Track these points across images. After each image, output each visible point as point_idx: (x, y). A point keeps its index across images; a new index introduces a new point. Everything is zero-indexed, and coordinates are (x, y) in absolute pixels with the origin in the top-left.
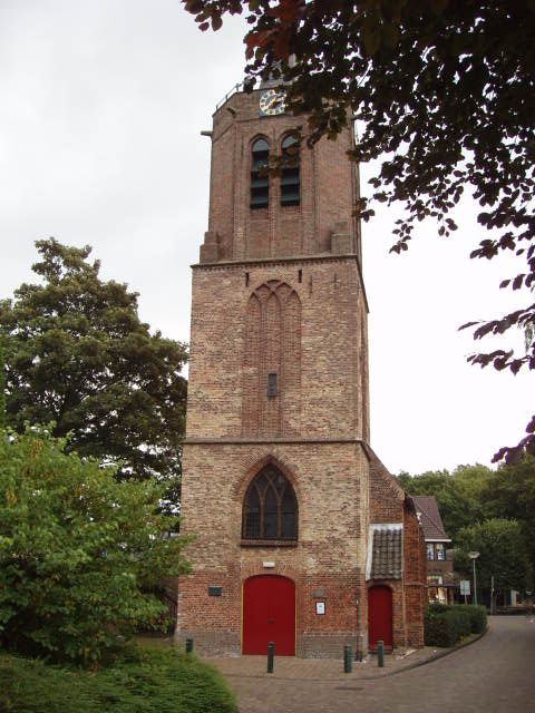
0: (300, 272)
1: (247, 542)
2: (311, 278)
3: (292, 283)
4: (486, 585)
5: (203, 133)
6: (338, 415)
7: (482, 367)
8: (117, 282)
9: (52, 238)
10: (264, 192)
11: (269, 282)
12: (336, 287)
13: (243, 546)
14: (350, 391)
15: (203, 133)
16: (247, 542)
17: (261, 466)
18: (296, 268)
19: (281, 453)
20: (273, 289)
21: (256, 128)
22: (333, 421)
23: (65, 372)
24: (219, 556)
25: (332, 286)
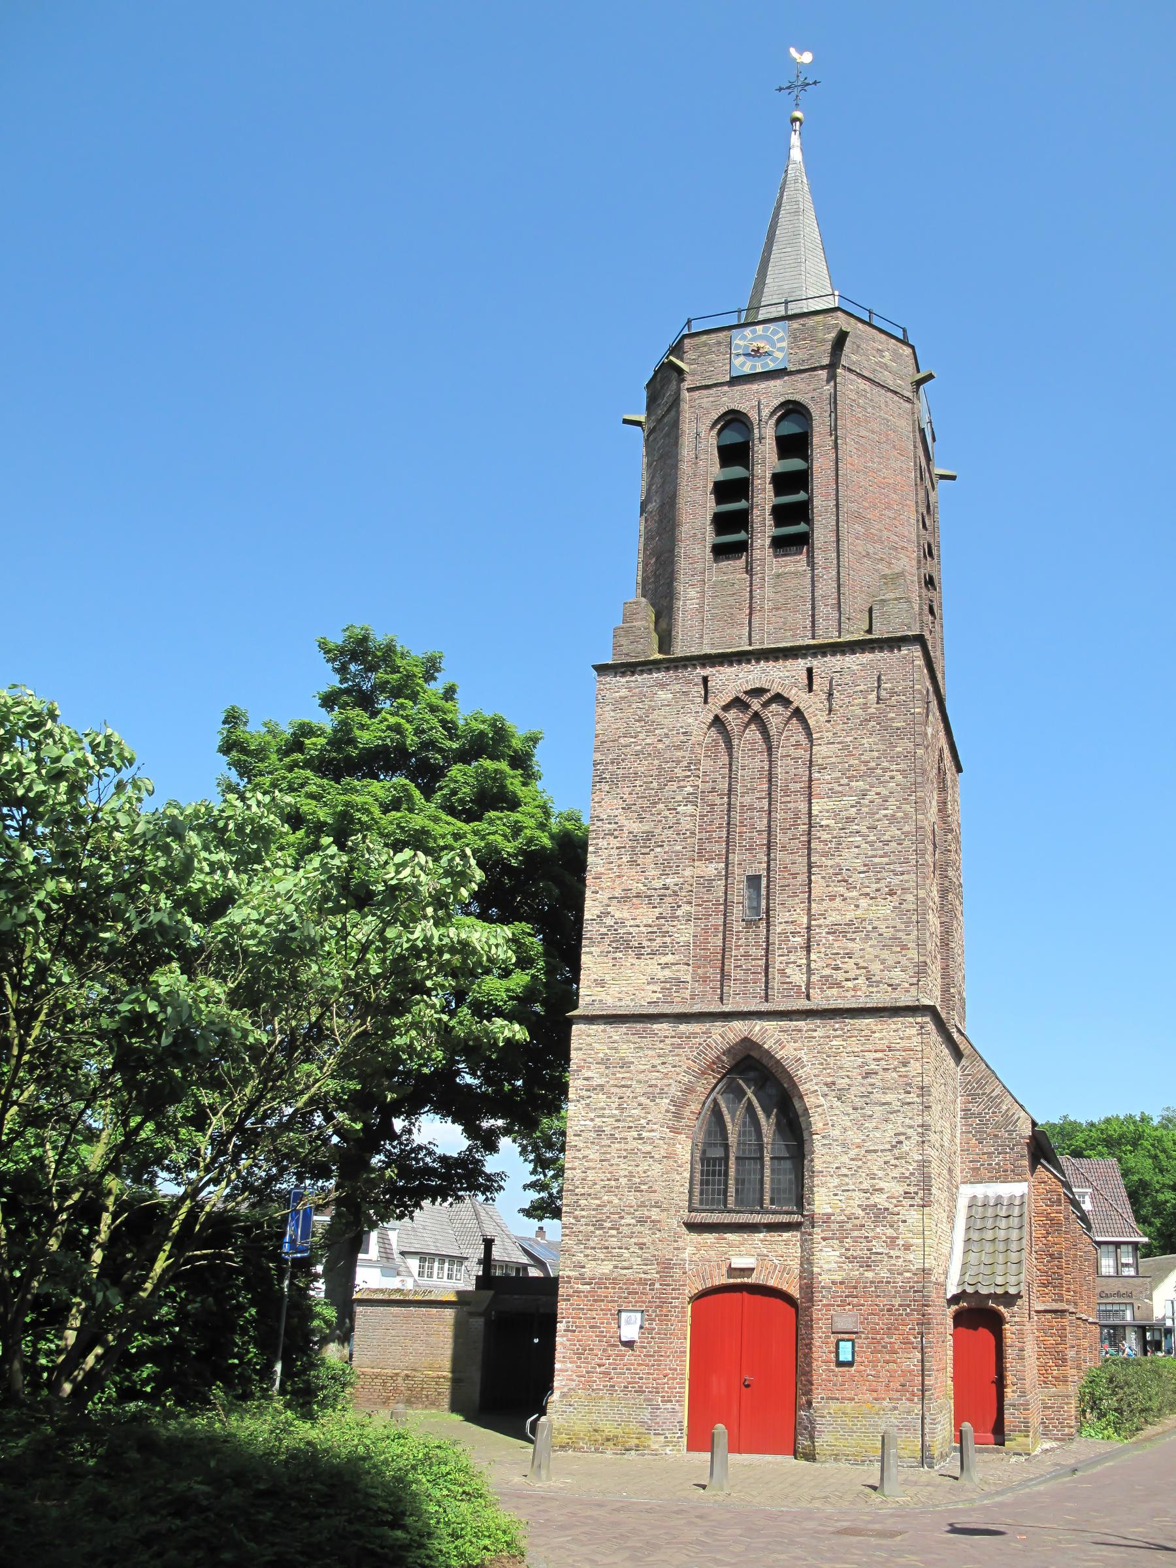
0: (810, 671)
1: (700, 1217)
6: (885, 954)
13: (692, 1227)
18: (801, 664)
22: (876, 967)
24: (641, 1246)
25: (873, 697)
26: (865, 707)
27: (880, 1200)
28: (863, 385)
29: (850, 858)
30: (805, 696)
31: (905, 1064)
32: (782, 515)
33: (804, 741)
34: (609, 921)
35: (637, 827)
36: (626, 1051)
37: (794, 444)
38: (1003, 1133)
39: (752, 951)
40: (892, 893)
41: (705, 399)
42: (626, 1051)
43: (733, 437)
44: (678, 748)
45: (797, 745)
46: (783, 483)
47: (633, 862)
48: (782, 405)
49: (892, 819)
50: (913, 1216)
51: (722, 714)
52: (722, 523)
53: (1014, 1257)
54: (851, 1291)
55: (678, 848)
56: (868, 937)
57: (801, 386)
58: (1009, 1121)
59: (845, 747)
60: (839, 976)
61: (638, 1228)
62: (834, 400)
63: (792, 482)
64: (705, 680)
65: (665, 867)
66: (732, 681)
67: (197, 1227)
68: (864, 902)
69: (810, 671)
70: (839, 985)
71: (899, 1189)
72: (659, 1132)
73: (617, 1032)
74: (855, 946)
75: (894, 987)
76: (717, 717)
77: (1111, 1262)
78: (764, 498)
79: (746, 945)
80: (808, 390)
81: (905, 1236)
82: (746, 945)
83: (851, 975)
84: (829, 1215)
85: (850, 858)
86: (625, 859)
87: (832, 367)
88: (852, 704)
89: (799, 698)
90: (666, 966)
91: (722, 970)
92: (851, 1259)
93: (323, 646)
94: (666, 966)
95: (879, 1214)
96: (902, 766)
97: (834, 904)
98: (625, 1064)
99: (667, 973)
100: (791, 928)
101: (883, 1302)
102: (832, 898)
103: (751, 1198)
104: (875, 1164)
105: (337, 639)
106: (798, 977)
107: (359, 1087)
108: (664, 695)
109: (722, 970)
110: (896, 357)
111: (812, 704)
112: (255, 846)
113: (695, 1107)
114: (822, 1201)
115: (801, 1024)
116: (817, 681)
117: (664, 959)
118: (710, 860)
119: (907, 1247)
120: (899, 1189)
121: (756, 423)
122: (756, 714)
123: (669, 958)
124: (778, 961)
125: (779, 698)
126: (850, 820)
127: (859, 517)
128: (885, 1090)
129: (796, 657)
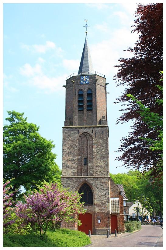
0: (93, 130)
6: (103, 170)
18: (91, 129)
22: (102, 172)
26: (100, 136)
27: (103, 202)
28: (99, 86)
29: (98, 157)
30: (92, 133)
31: (106, 184)
32: (88, 106)
34: (66, 164)
35: (69, 151)
36: (69, 182)
37: (90, 95)
38: (116, 191)
39: (85, 168)
40: (104, 162)
42: (69, 182)
43: (81, 93)
44: (75, 140)
47: (69, 156)
49: (104, 152)
50: (107, 204)
51: (81, 135)
52: (79, 106)
53: (114, 205)
54: (100, 214)
56: (101, 168)
57: (91, 86)
58: (117, 190)
59: (98, 141)
60: (97, 173)
63: (90, 101)
64: (78, 130)
65: (73, 157)
68: (100, 163)
69: (93, 130)
70: (97, 174)
71: (105, 201)
74: (100, 168)
76: (80, 136)
77: (126, 204)
78: (86, 104)
79: (84, 168)
81: (106, 207)
83: (99, 172)
84: (97, 204)
85: (98, 157)
86: (68, 155)
88: (98, 135)
90: (74, 170)
92: (99, 209)
93: (13, 116)
94: (74, 170)
95: (103, 204)
97: (97, 163)
98: (69, 184)
99: (74, 171)
100: (90, 166)
101: (103, 215)
102: (96, 162)
104: (102, 197)
107: (15, 178)
108: (72, 132)
110: (104, 80)
111: (93, 135)
114: (96, 202)
115: (92, 179)
116: (94, 132)
118: (79, 156)
119: (107, 208)
120: (105, 201)
122: (85, 136)
123: (74, 169)
126: (98, 151)
127: (99, 107)
128: (104, 188)
129: (91, 128)
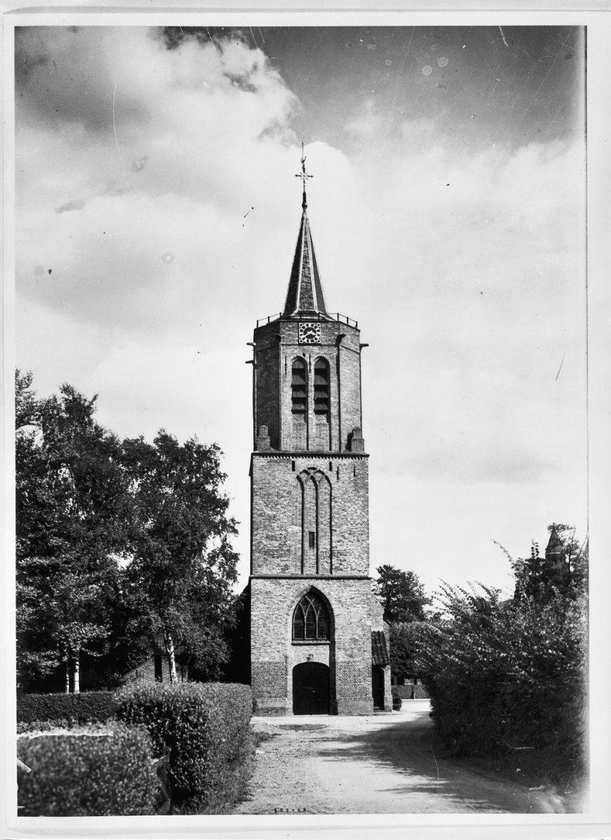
0: (330, 463)
1: (295, 642)
2: (338, 468)
3: (325, 471)
4: (313, 627)
5: (248, 344)
6: (356, 561)
7: (142, 438)
8: (130, 438)
9: (67, 390)
10: (304, 401)
11: (309, 469)
12: (355, 476)
13: (293, 644)
14: (365, 546)
15: (248, 344)
16: (295, 642)
17: (305, 593)
18: (327, 461)
19: (320, 585)
20: (312, 474)
21: (296, 351)
22: (353, 565)
23: (387, 586)
24: (279, 652)
25: (352, 474)
33: (329, 488)
41: (289, 351)
45: (326, 488)
46: (318, 388)
48: (318, 357)
55: (286, 521)
60: (342, 567)
61: (278, 646)
62: (338, 357)
63: (323, 389)
66: (302, 463)
67: (67, 676)
69: (330, 463)
70: (342, 570)
72: (283, 613)
73: (267, 583)
75: (359, 571)
79: (310, 554)
80: (329, 354)
82: (310, 554)
87: (337, 345)
89: (328, 473)
91: (331, 495)
96: (362, 499)
103: (312, 634)
105: (45, 390)
106: (327, 566)
109: (331, 495)
112: (164, 501)
113: (294, 607)
117: (282, 559)
121: (308, 363)
124: (321, 561)
125: (320, 471)
